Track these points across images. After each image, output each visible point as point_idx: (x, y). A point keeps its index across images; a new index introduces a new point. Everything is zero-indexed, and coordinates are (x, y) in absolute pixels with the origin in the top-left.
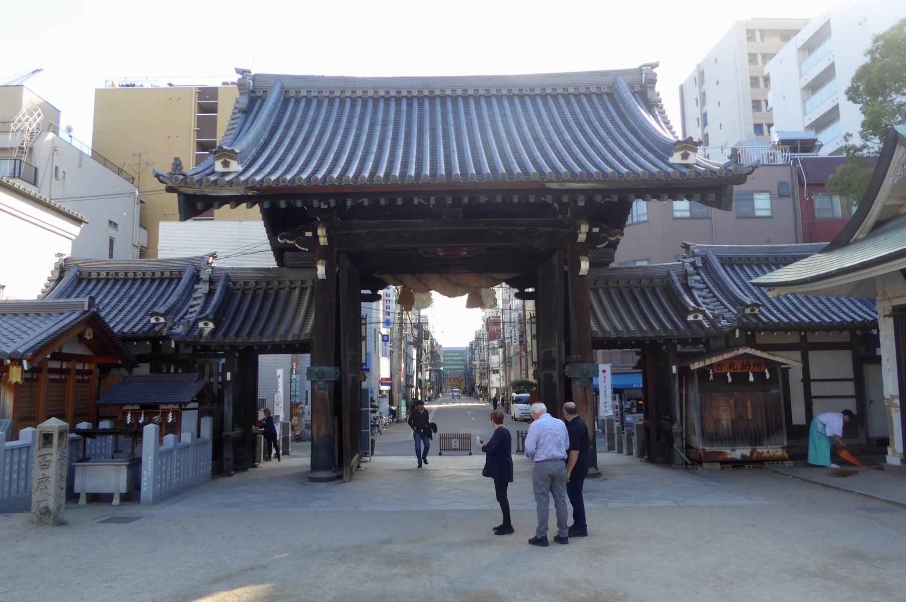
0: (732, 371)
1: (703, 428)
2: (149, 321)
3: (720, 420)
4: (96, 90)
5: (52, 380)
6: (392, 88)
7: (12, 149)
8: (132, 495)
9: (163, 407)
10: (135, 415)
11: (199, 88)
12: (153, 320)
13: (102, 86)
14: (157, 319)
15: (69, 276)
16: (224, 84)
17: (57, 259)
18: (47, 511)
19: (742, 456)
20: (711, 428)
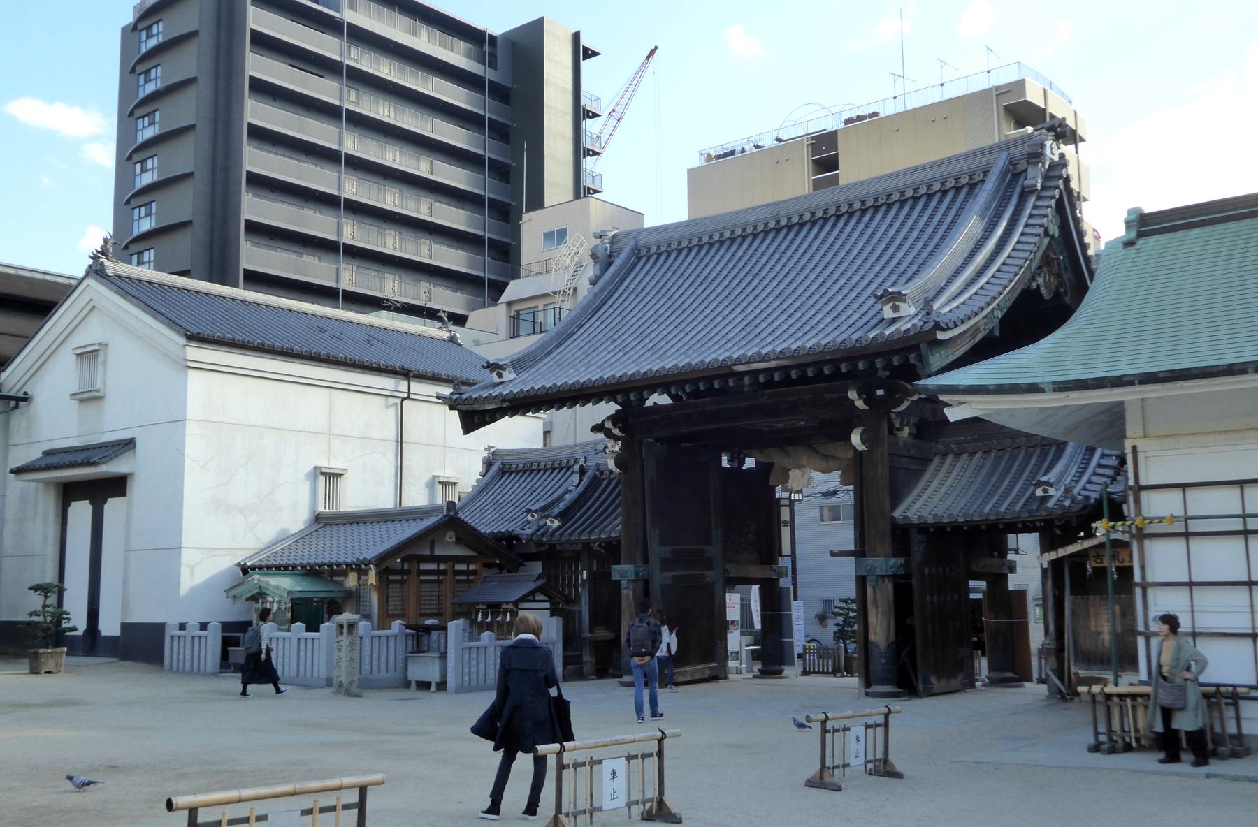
0: (1118, 564)
1: (1076, 644)
2: (1033, 493)
3: (1099, 633)
4: (689, 171)
5: (458, 581)
6: (724, 229)
7: (555, 293)
8: (442, 686)
9: (504, 606)
10: (485, 615)
11: (813, 138)
12: (1039, 493)
13: (696, 162)
14: (1045, 491)
15: (494, 469)
16: (848, 121)
17: (486, 454)
18: (341, 685)
19: (536, 621)
20: (1087, 644)
